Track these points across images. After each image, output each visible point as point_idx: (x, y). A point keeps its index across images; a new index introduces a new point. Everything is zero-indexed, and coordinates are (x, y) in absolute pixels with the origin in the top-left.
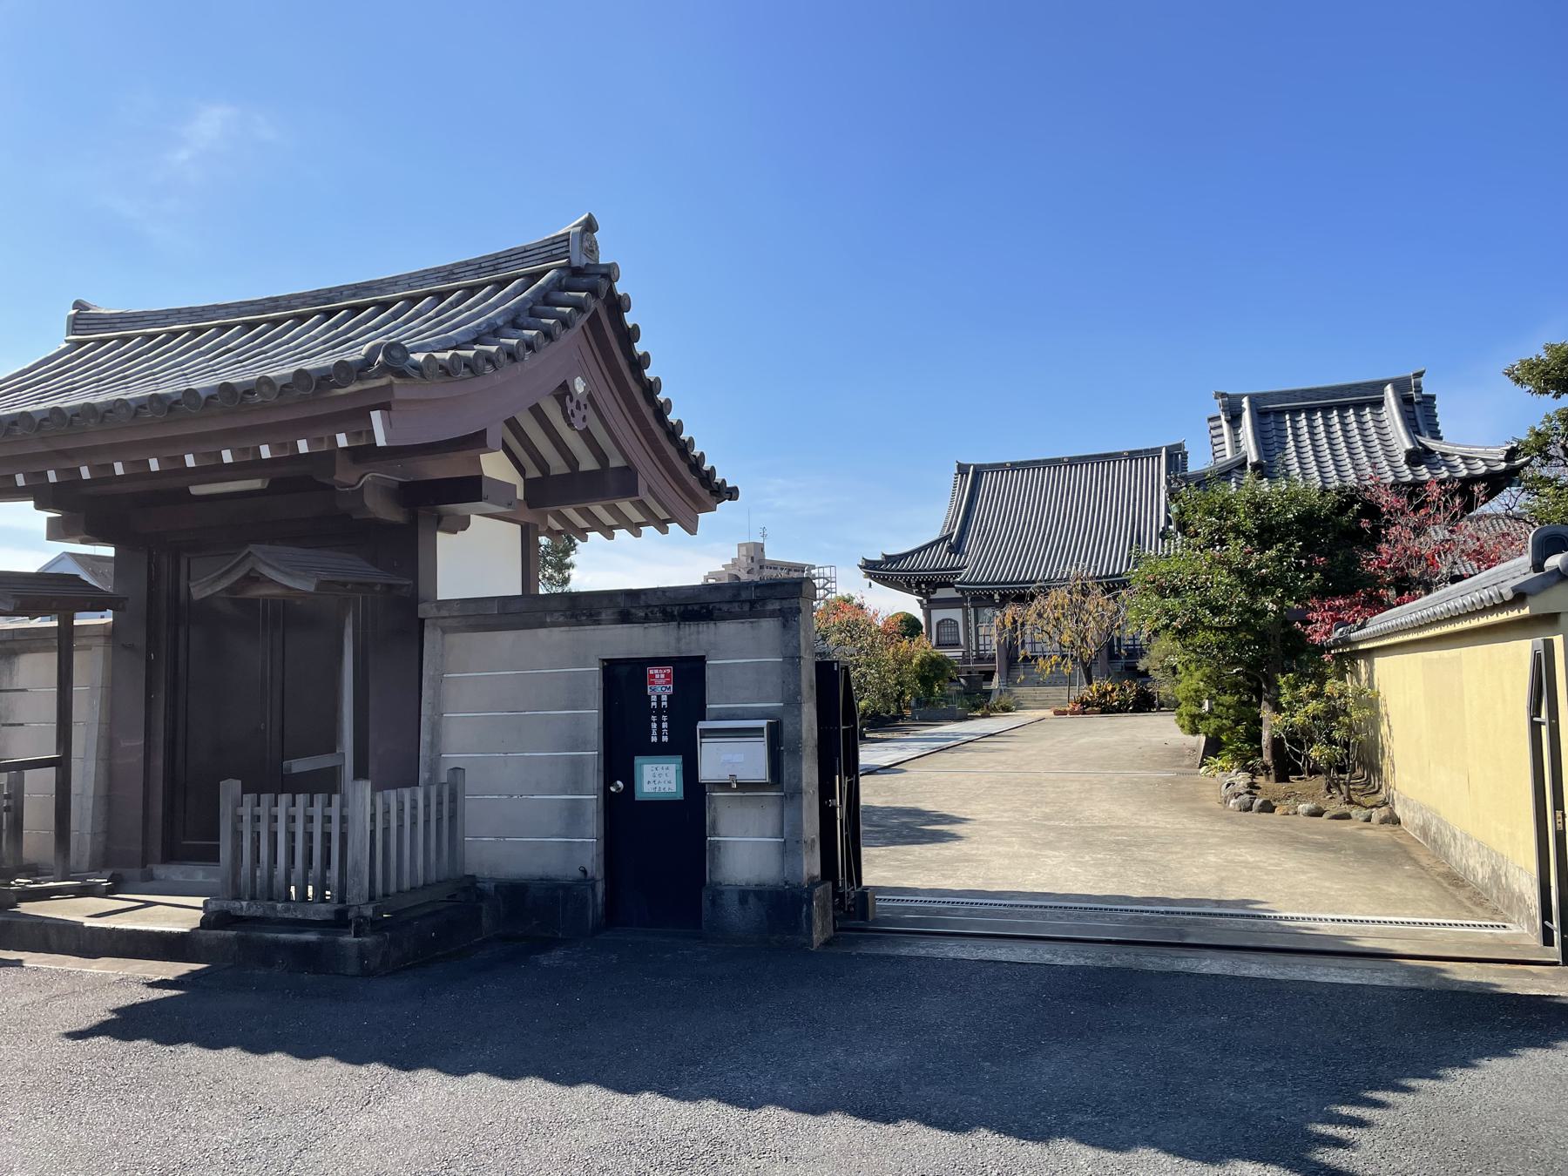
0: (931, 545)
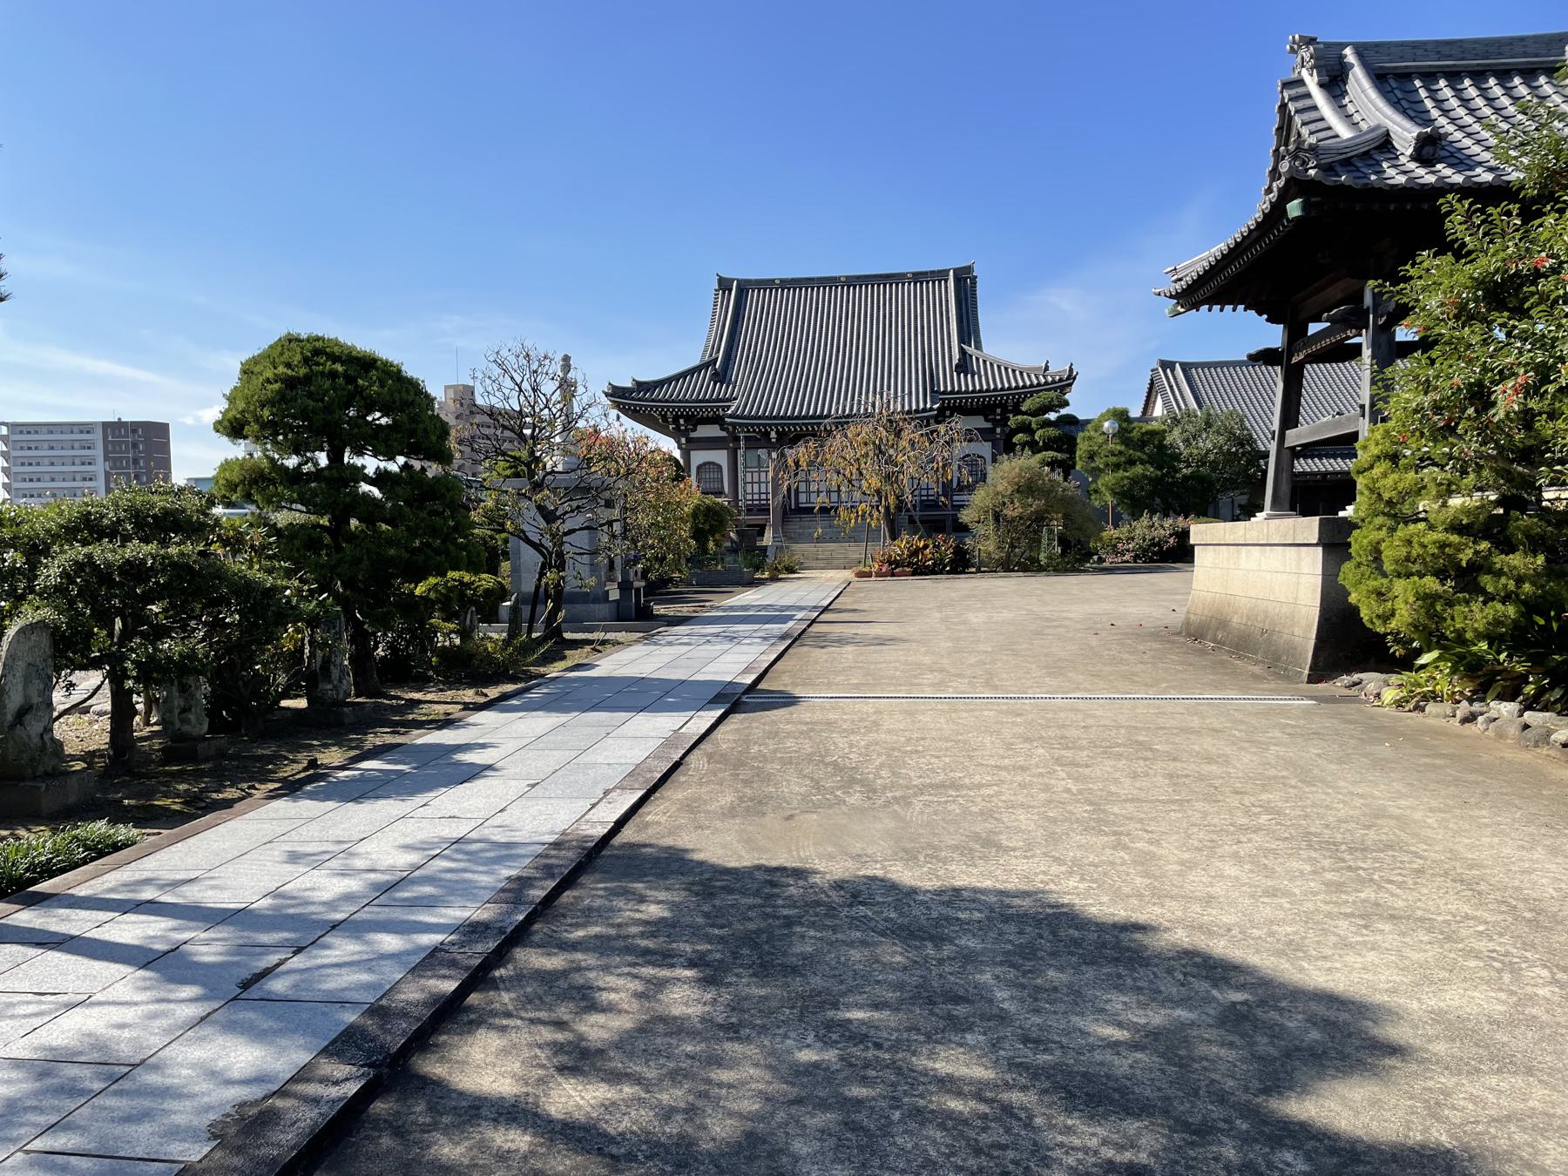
0: (691, 372)
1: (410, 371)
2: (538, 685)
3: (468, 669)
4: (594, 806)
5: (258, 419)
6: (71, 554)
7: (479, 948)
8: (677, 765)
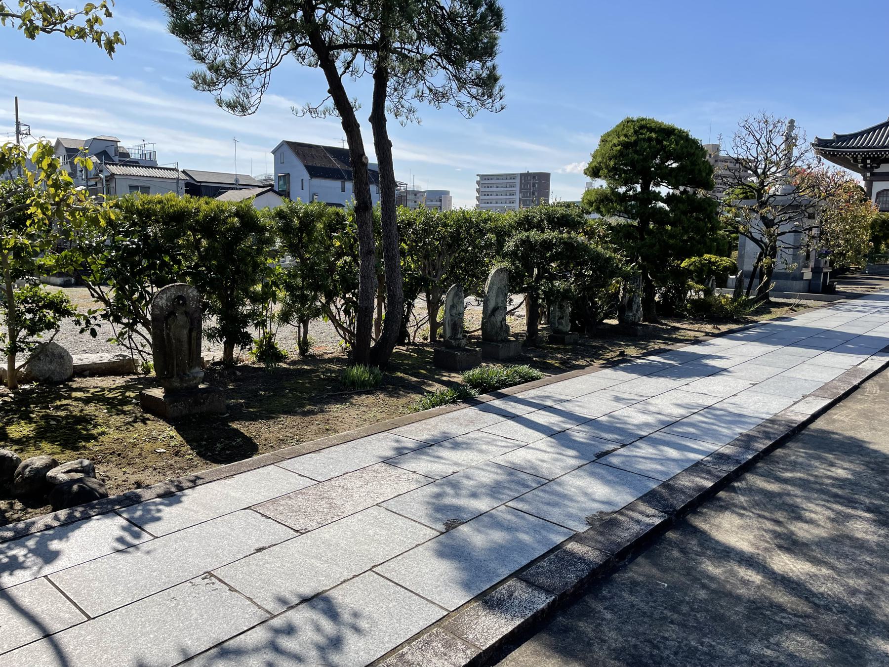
1: (693, 135)
2: (754, 327)
3: (707, 312)
4: (795, 403)
5: (607, 167)
6: (520, 236)
7: (725, 468)
8: (855, 388)
